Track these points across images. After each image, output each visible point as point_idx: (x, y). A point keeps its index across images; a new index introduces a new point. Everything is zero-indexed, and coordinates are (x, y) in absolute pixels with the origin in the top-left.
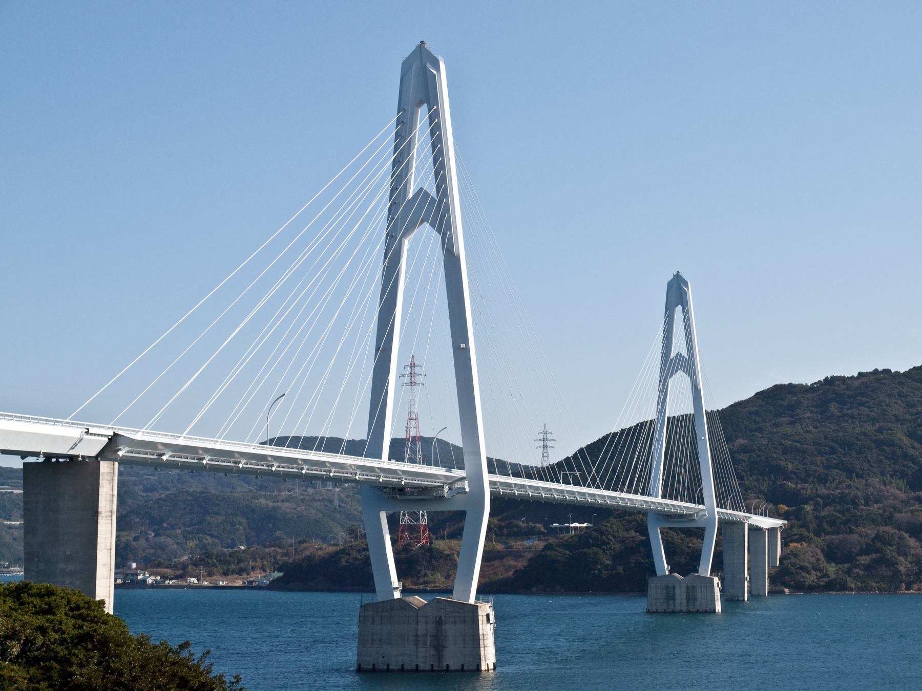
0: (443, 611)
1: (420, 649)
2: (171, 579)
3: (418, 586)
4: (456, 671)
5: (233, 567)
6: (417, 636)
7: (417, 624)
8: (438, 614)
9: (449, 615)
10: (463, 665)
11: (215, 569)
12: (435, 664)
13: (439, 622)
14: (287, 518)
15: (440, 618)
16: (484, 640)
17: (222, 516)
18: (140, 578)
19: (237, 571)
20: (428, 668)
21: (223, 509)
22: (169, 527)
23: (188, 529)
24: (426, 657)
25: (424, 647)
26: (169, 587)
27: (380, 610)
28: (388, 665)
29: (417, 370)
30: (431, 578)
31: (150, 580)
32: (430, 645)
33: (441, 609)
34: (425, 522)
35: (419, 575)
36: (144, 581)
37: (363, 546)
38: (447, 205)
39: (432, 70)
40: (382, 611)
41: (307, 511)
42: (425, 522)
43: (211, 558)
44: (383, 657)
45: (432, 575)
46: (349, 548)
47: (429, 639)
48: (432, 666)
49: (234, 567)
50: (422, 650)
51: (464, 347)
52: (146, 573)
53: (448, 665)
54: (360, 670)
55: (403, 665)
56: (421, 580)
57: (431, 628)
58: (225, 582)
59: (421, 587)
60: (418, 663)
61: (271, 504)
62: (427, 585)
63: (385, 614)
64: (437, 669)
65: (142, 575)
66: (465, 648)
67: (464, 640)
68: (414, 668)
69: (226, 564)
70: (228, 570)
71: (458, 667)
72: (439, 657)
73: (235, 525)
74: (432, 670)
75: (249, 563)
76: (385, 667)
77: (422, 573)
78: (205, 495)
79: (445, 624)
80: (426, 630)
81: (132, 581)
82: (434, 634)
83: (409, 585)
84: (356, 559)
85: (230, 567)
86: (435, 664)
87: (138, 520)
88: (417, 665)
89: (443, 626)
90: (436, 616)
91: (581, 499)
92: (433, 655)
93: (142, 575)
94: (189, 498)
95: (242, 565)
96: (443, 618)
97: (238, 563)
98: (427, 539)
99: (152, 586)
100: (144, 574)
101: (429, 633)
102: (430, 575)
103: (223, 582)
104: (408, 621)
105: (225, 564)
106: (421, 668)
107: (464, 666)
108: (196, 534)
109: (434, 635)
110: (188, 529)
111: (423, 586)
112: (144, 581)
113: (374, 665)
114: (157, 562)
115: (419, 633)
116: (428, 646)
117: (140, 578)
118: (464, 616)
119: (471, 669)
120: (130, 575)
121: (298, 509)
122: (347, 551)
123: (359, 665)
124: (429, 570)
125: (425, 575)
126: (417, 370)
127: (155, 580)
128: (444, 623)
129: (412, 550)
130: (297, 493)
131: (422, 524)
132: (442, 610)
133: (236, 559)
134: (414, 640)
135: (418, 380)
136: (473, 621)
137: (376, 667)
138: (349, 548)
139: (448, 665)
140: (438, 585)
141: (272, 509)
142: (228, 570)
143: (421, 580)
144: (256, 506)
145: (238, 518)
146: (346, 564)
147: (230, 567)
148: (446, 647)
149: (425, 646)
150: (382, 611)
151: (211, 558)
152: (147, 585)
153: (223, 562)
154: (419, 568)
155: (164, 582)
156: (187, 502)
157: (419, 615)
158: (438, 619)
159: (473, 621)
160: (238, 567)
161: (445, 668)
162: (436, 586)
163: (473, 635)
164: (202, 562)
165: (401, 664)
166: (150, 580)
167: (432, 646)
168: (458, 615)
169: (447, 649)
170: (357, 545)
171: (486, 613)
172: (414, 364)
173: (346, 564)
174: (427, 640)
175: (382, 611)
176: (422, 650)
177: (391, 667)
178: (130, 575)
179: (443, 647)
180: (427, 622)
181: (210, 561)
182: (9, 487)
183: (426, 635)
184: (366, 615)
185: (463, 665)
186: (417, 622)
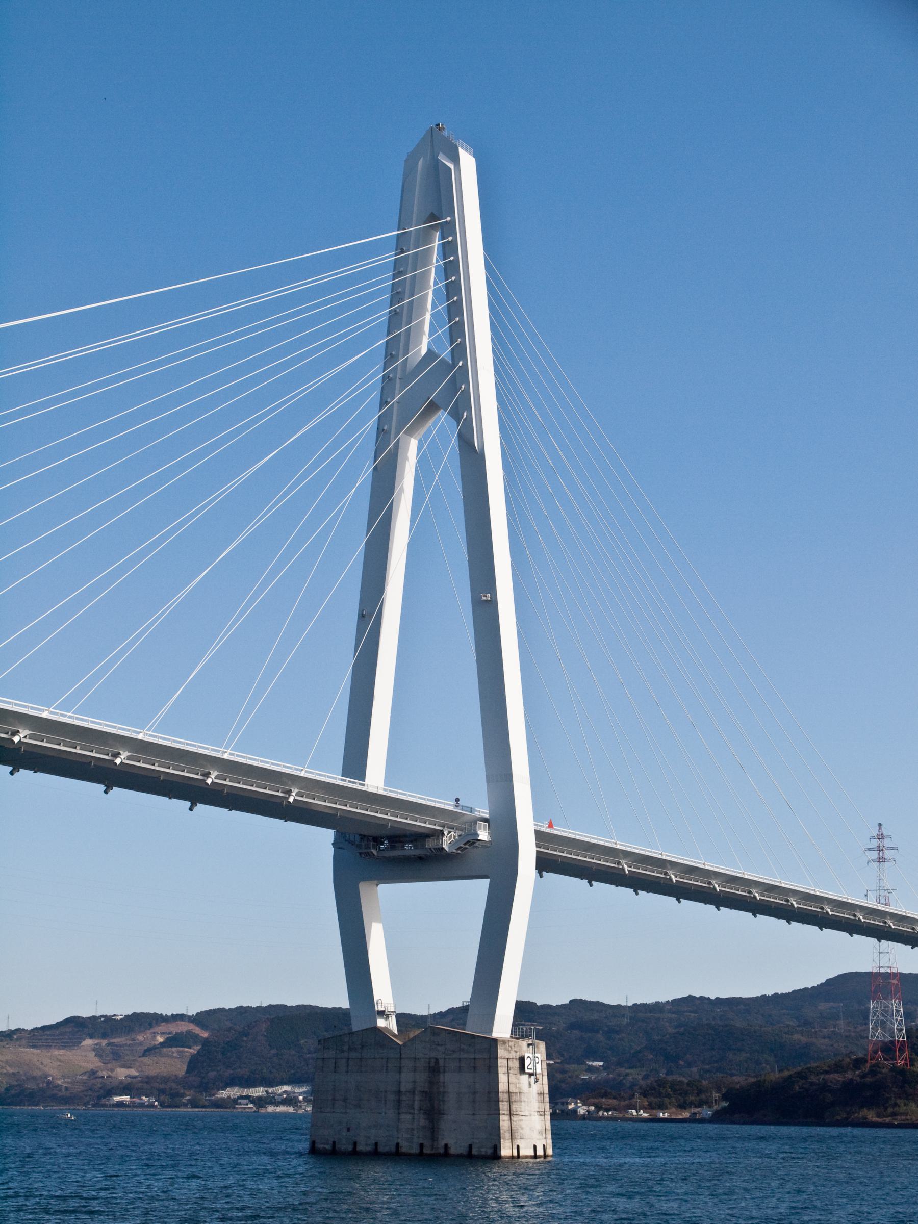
0: (441, 1049)
1: (403, 1117)
2: (607, 1110)
3: (884, 1119)
4: (460, 1156)
5: (691, 1098)
6: (399, 1092)
7: (400, 1072)
8: (433, 1055)
9: (451, 1057)
10: (470, 1147)
11: (667, 1100)
12: (427, 1143)
13: (434, 1069)
14: (821, 1056)
15: (437, 1061)
16: (510, 1102)
17: (747, 1053)
18: (570, 1107)
19: (696, 1103)
20: (415, 1150)
21: (748, 1044)
22: (686, 1065)
23: (707, 1067)
24: (413, 1129)
25: (410, 1113)
26: (603, 1118)
27: (346, 1048)
28: (355, 1144)
29: (887, 843)
30: (903, 1109)
31: (582, 1111)
32: (420, 1109)
33: (438, 1045)
34: (903, 1038)
35: (888, 1105)
36: (574, 1111)
37: (824, 1068)
38: (465, 368)
39: (443, 161)
40: (350, 1049)
41: (846, 1048)
42: (903, 1038)
43: (664, 1087)
44: (348, 1130)
45: (905, 1105)
46: (806, 1071)
47: (417, 1098)
48: (422, 1146)
49: (693, 1098)
50: (405, 1117)
51: (489, 598)
52: (579, 1101)
53: (446, 1145)
54: (314, 1151)
55: (376, 1144)
56: (890, 1110)
57: (422, 1078)
58: (666, 1114)
59: (888, 1120)
60: (399, 1141)
61: (804, 1040)
62: (895, 1117)
63: (353, 1055)
64: (429, 1152)
65: (573, 1104)
66: (474, 1114)
67: (474, 1101)
68: (393, 1149)
69: (683, 1095)
70: (685, 1102)
71: (463, 1150)
72: (433, 1131)
73: (761, 1064)
74: (421, 1154)
75: (711, 1094)
76: (350, 1148)
77: (892, 1102)
78: (728, 1028)
79: (444, 1072)
80: (415, 1082)
81: (562, 1111)
82: (427, 1090)
83: (872, 1117)
84: (812, 1084)
85: (687, 1098)
86: (427, 1143)
87: (652, 1056)
88: (398, 1144)
89: (441, 1076)
90: (430, 1058)
91: (833, 913)
92: (424, 1127)
93: (573, 1104)
94: (710, 1031)
95: (703, 1096)
96: (441, 1063)
97: (698, 1095)
98: (906, 1060)
99: (583, 1118)
100: (576, 1103)
101: (419, 1089)
102: (902, 1104)
103: (664, 1113)
104: (387, 1067)
105: (681, 1094)
106: (404, 1150)
107: (473, 1146)
108: (714, 1074)
109: (426, 1092)
110: (707, 1067)
111: (890, 1118)
112: (574, 1111)
113: (334, 1143)
114: (603, 1091)
115: (403, 1089)
116: (416, 1112)
117: (570, 1107)
118: (475, 1059)
119: (483, 1153)
120: (560, 1104)
121: (836, 1046)
122: (803, 1074)
123: (313, 1143)
124: (900, 1098)
125: (896, 1105)
126: (887, 843)
127: (588, 1111)
128: (441, 1070)
129: (881, 1073)
130: (841, 1028)
131: (898, 1041)
132: (439, 1048)
133: (695, 1088)
134: (394, 1100)
135: (888, 854)
136: (489, 1067)
137: (337, 1146)
138: (806, 1071)
139: (446, 1145)
140: (909, 1117)
141: (805, 1046)
142: (685, 1102)
143: (890, 1110)
144: (786, 1042)
145: (765, 1056)
146: (800, 1090)
147: (687, 1098)
148: (443, 1114)
149: (411, 1111)
150: (349, 1049)
151: (664, 1087)
152: (578, 1116)
153: (679, 1092)
154: (888, 1096)
155: (598, 1113)
156: (707, 1037)
157: (403, 1056)
158: (432, 1064)
159: (489, 1067)
160: (697, 1098)
161: (442, 1151)
162: (908, 1120)
163: (489, 1093)
164: (653, 1092)
165: (374, 1142)
166: (582, 1111)
167: (422, 1112)
168: (465, 1056)
169: (445, 1117)
170: (817, 1067)
171: (518, 1055)
172: (882, 835)
173: (800, 1090)
174: (414, 1101)
175: (350, 1049)
176: (405, 1117)
177: (359, 1148)
178: (560, 1104)
179: (441, 1113)
180: (415, 1070)
181: (663, 1091)
182: (536, 1023)
183: (414, 1092)
184: (325, 1056)
185: (470, 1147)
186: (400, 1068)
